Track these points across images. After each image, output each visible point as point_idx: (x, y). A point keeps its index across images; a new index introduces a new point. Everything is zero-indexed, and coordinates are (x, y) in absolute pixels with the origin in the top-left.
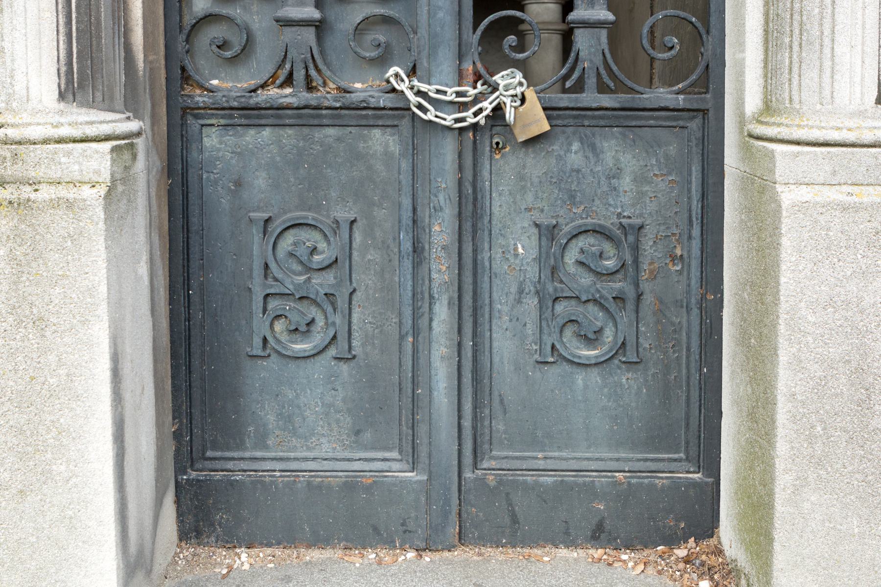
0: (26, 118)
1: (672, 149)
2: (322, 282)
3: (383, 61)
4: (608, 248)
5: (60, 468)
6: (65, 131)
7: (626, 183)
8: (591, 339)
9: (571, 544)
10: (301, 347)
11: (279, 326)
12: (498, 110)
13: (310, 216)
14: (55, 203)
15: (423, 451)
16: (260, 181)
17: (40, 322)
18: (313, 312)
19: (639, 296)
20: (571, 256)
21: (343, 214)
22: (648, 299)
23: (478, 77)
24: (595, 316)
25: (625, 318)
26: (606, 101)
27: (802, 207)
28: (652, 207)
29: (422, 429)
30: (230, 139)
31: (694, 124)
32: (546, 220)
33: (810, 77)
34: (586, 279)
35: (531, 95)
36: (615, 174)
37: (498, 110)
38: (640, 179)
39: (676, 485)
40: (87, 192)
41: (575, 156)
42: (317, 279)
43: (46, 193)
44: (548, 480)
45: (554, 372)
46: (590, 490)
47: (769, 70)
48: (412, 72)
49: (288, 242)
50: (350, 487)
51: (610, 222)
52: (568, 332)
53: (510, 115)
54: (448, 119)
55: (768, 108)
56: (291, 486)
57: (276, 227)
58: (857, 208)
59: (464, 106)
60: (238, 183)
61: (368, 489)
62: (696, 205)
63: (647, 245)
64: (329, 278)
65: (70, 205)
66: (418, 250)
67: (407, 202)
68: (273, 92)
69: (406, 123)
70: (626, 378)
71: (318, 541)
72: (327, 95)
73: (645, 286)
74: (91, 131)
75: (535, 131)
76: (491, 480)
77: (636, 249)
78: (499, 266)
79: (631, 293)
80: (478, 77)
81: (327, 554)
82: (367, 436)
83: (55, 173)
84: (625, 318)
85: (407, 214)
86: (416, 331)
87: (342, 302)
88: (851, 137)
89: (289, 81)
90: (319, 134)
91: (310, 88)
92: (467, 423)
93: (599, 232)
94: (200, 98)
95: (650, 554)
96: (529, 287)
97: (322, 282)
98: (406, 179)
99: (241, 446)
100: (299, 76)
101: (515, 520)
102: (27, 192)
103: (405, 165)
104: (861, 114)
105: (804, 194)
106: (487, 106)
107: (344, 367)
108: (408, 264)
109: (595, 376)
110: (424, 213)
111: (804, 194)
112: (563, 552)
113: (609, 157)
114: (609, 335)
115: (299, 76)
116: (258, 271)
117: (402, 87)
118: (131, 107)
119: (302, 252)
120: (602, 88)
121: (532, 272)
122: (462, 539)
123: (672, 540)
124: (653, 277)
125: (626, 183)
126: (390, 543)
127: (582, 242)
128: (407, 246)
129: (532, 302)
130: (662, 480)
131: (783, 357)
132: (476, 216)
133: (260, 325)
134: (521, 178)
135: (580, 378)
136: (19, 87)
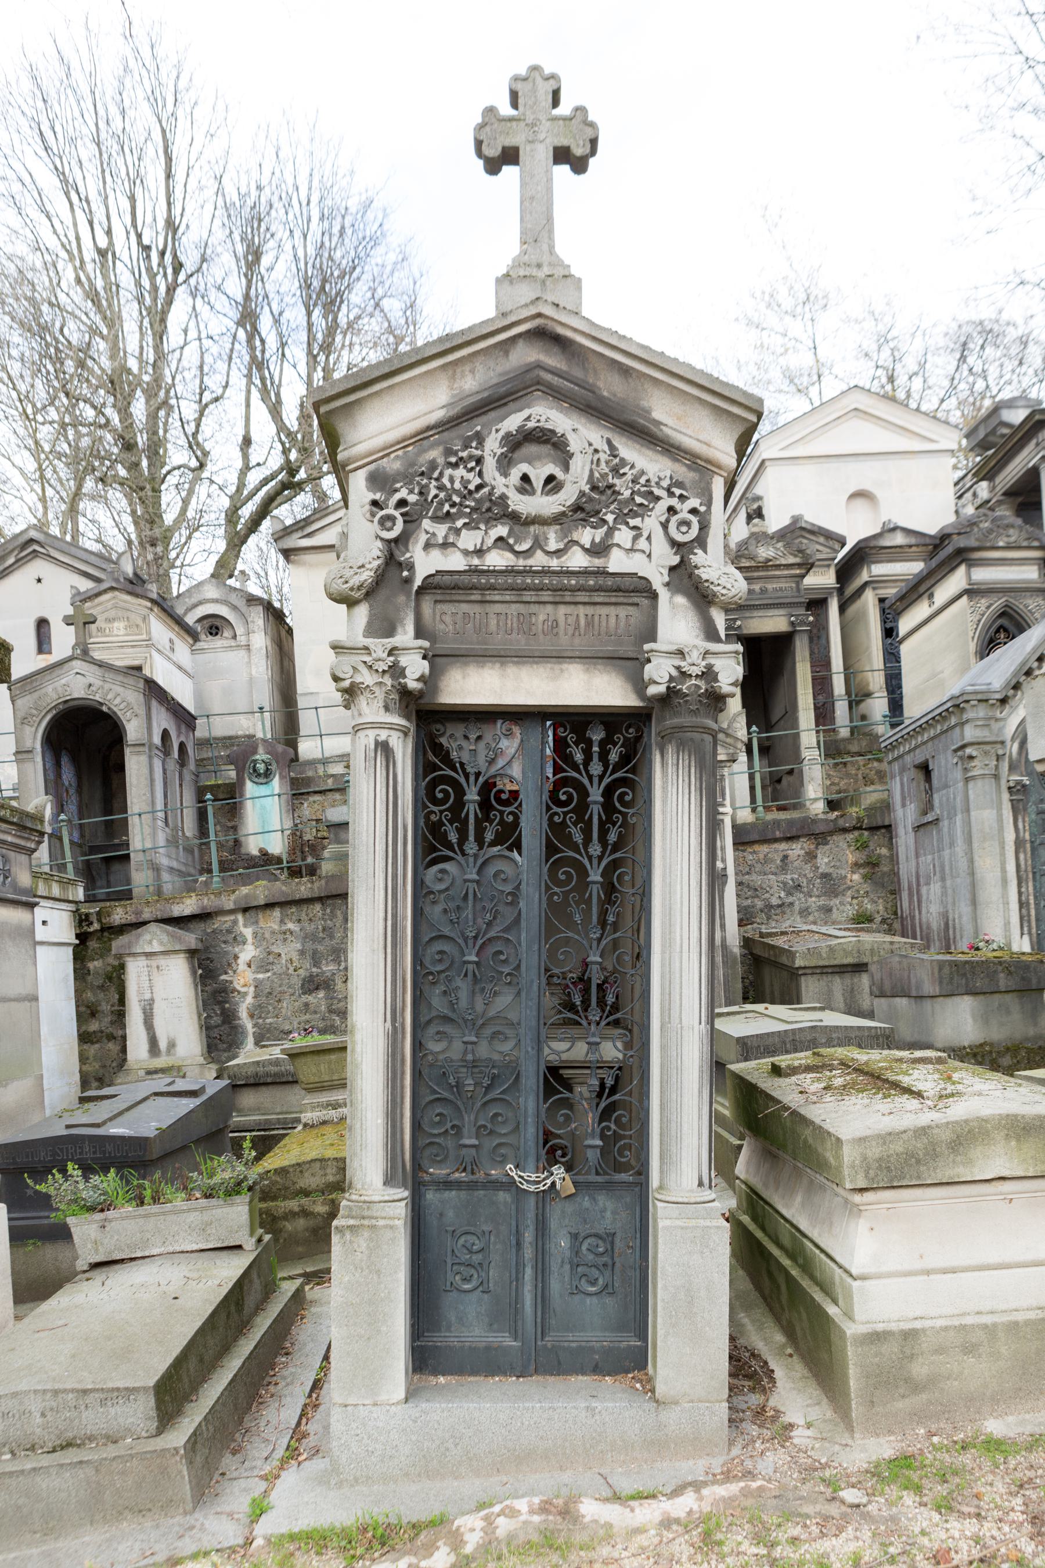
0: (370, 1192)
1: (628, 1200)
2: (476, 1258)
3: (503, 1162)
4: (600, 1242)
5: (384, 1329)
6: (387, 1198)
7: (608, 1214)
8: (593, 1283)
9: (584, 1374)
10: (467, 1287)
11: (457, 1278)
12: (553, 1184)
13: (472, 1229)
14: (386, 1226)
15: (520, 1332)
16: (450, 1214)
17: (378, 1272)
18: (473, 1271)
19: (614, 1264)
20: (584, 1247)
21: (486, 1228)
22: (618, 1265)
23: (544, 1169)
24: (595, 1273)
25: (608, 1273)
26: (599, 1179)
27: (666, 1228)
28: (619, 1225)
29: (520, 1323)
30: (438, 1195)
31: (637, 1189)
32: (573, 1231)
33: (673, 1175)
34: (591, 1257)
35: (567, 1178)
36: (603, 1211)
37: (553, 1184)
38: (614, 1213)
39: (629, 1347)
40: (397, 1222)
41: (586, 1202)
42: (474, 1257)
43: (381, 1223)
44: (574, 1345)
45: (577, 1298)
46: (592, 1350)
47: (662, 1172)
48: (517, 1167)
49: (462, 1241)
50: (488, 1348)
51: (601, 1232)
52: (583, 1280)
53: (558, 1187)
54: (532, 1188)
55: (661, 1187)
56: (462, 1348)
57: (458, 1233)
58: (687, 1228)
59: (539, 1183)
60: (441, 1215)
61: (496, 1349)
62: (638, 1224)
63: (617, 1241)
64: (480, 1256)
65: (391, 1227)
66: (519, 1244)
67: (514, 1223)
68: (457, 1175)
69: (514, 1189)
70: (608, 1300)
71: (474, 1373)
72: (480, 1176)
73: (616, 1259)
74: (396, 1197)
75: (569, 1193)
76: (549, 1345)
77: (612, 1243)
78: (553, 1251)
79: (610, 1263)
80: (544, 1169)
81: (477, 1378)
82: (495, 1326)
83: (384, 1215)
84: (608, 1273)
85: (514, 1229)
86: (517, 1280)
87: (485, 1267)
88: (686, 1200)
89: (464, 1170)
90: (476, 1193)
91: (473, 1173)
92: (539, 1320)
93: (596, 1235)
94: (427, 1178)
95: (619, 1377)
96: (566, 1260)
97: (476, 1258)
98: (513, 1213)
99: (440, 1331)
100: (469, 1168)
101: (559, 1363)
102: (374, 1222)
103: (513, 1207)
104: (692, 1191)
105: (668, 1222)
106: (549, 1182)
107: (486, 1296)
108: (514, 1250)
109: (595, 1299)
110: (521, 1228)
111: (668, 1222)
112: (580, 1377)
113: (601, 1203)
114: (601, 1281)
115: (469, 1168)
116: (449, 1253)
117: (513, 1174)
118: (404, 1186)
119: (468, 1245)
120: (597, 1173)
121: (568, 1253)
122: (536, 1372)
123: (627, 1372)
124: (620, 1255)
125: (608, 1214)
126: (505, 1374)
127: (589, 1240)
128: (514, 1242)
129: (567, 1267)
130: (624, 1345)
131: (660, 1285)
132: (544, 1229)
133: (450, 1276)
134: (563, 1212)
135: (588, 1300)
136: (368, 1180)
